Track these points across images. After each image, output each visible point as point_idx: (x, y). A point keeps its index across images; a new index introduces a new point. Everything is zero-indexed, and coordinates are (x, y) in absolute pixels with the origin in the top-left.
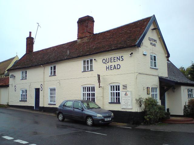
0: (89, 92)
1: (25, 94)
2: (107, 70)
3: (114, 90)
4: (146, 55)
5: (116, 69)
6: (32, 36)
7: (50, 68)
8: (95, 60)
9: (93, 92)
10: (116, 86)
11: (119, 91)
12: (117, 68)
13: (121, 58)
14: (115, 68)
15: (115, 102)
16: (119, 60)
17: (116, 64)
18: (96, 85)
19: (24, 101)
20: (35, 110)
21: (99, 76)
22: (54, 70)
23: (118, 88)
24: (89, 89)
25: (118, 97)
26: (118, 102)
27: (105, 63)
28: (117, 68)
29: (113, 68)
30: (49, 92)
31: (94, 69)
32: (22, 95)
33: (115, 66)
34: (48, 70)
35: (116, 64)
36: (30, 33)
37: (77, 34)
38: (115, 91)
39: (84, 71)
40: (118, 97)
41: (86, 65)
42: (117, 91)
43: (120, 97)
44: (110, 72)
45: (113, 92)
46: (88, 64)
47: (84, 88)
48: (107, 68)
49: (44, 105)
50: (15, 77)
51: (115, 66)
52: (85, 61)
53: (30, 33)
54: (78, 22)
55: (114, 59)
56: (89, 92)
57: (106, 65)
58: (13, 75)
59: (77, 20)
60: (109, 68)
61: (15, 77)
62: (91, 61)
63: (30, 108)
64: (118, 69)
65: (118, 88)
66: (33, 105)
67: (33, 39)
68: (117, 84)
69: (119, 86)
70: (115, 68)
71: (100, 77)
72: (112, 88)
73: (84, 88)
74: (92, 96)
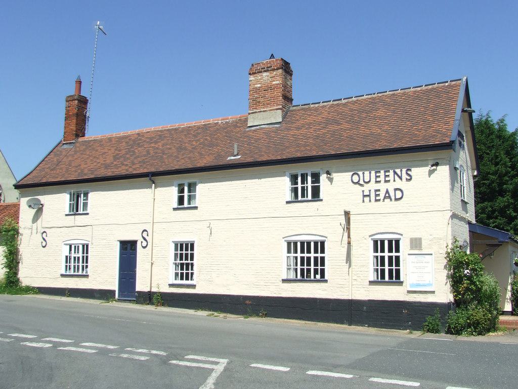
0: (306, 255)
1: (80, 255)
2: (363, 201)
3: (296, 252)
4: (429, 177)
5: (391, 199)
7: (6, 202)
9: (319, 255)
12: (393, 198)
13: (407, 174)
14: (387, 196)
16: (401, 178)
17: (391, 187)
18: (140, 239)
20: (119, 300)
21: (347, 214)
22: (313, 182)
23: (395, 245)
24: (305, 246)
26: (395, 278)
27: (358, 183)
28: (393, 198)
29: (382, 197)
32: (68, 259)
33: (387, 192)
35: (391, 187)
36: (79, 83)
38: (312, 255)
39: (295, 200)
41: (300, 186)
42: (308, 255)
43: (401, 268)
44: (372, 206)
45: (379, 254)
47: (292, 246)
48: (364, 196)
51: (387, 192)
53: (79, 83)
55: (386, 176)
56: (306, 255)
57: (362, 188)
58: (39, 200)
60: (369, 196)
63: (106, 295)
64: (396, 199)
65: (395, 245)
66: (113, 283)
69: (397, 242)
70: (389, 197)
71: (352, 218)
72: (378, 245)
73: (292, 246)
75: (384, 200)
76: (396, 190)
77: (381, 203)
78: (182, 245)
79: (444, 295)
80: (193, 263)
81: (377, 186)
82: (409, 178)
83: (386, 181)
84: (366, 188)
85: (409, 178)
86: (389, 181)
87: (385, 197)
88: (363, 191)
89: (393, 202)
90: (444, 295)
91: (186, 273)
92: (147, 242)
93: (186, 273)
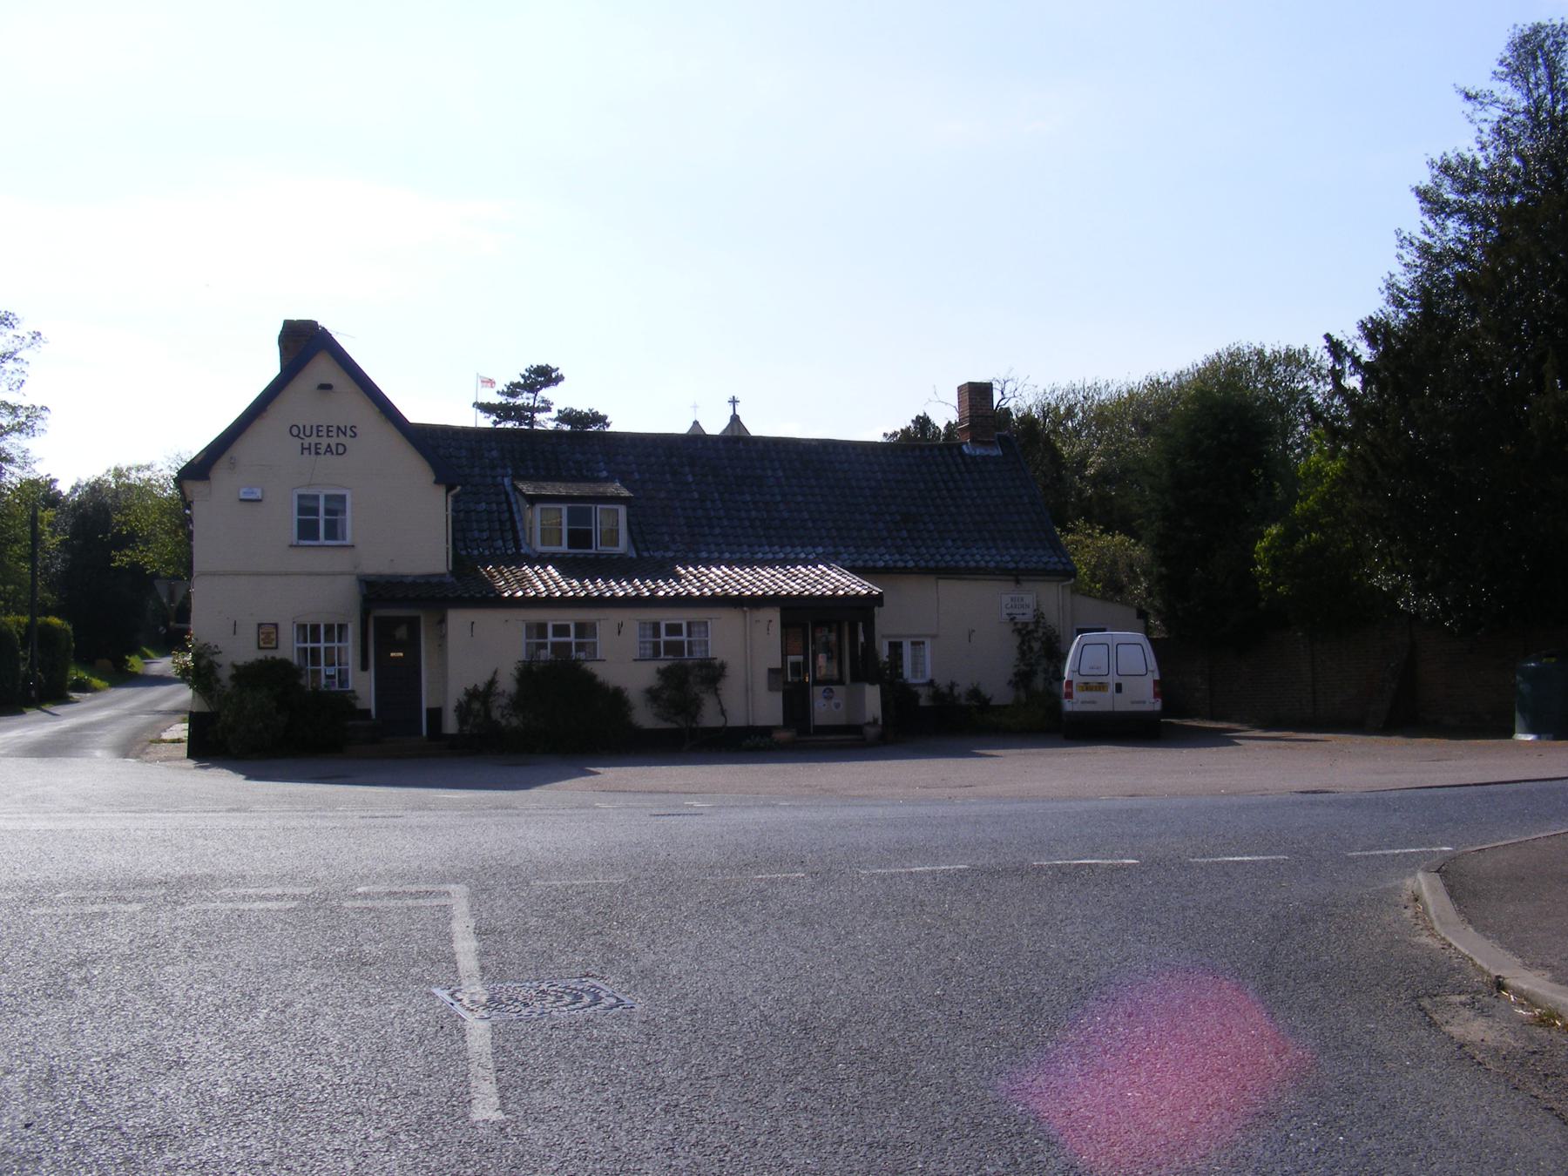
5: (333, 454)
14: (329, 449)
28: (335, 452)
33: (329, 446)
48: (303, 449)
51: (329, 446)
60: (310, 449)
64: (337, 454)
70: (331, 451)
75: (325, 454)
76: (338, 444)
77: (322, 456)
78: (315, 628)
79: (1153, 705)
80: (555, 627)
81: (318, 440)
82: (353, 435)
83: (328, 436)
84: (307, 442)
85: (353, 435)
86: (322, 436)
87: (326, 451)
88: (302, 444)
89: (335, 457)
90: (1153, 705)
91: (319, 642)
92: (726, 719)
93: (319, 642)
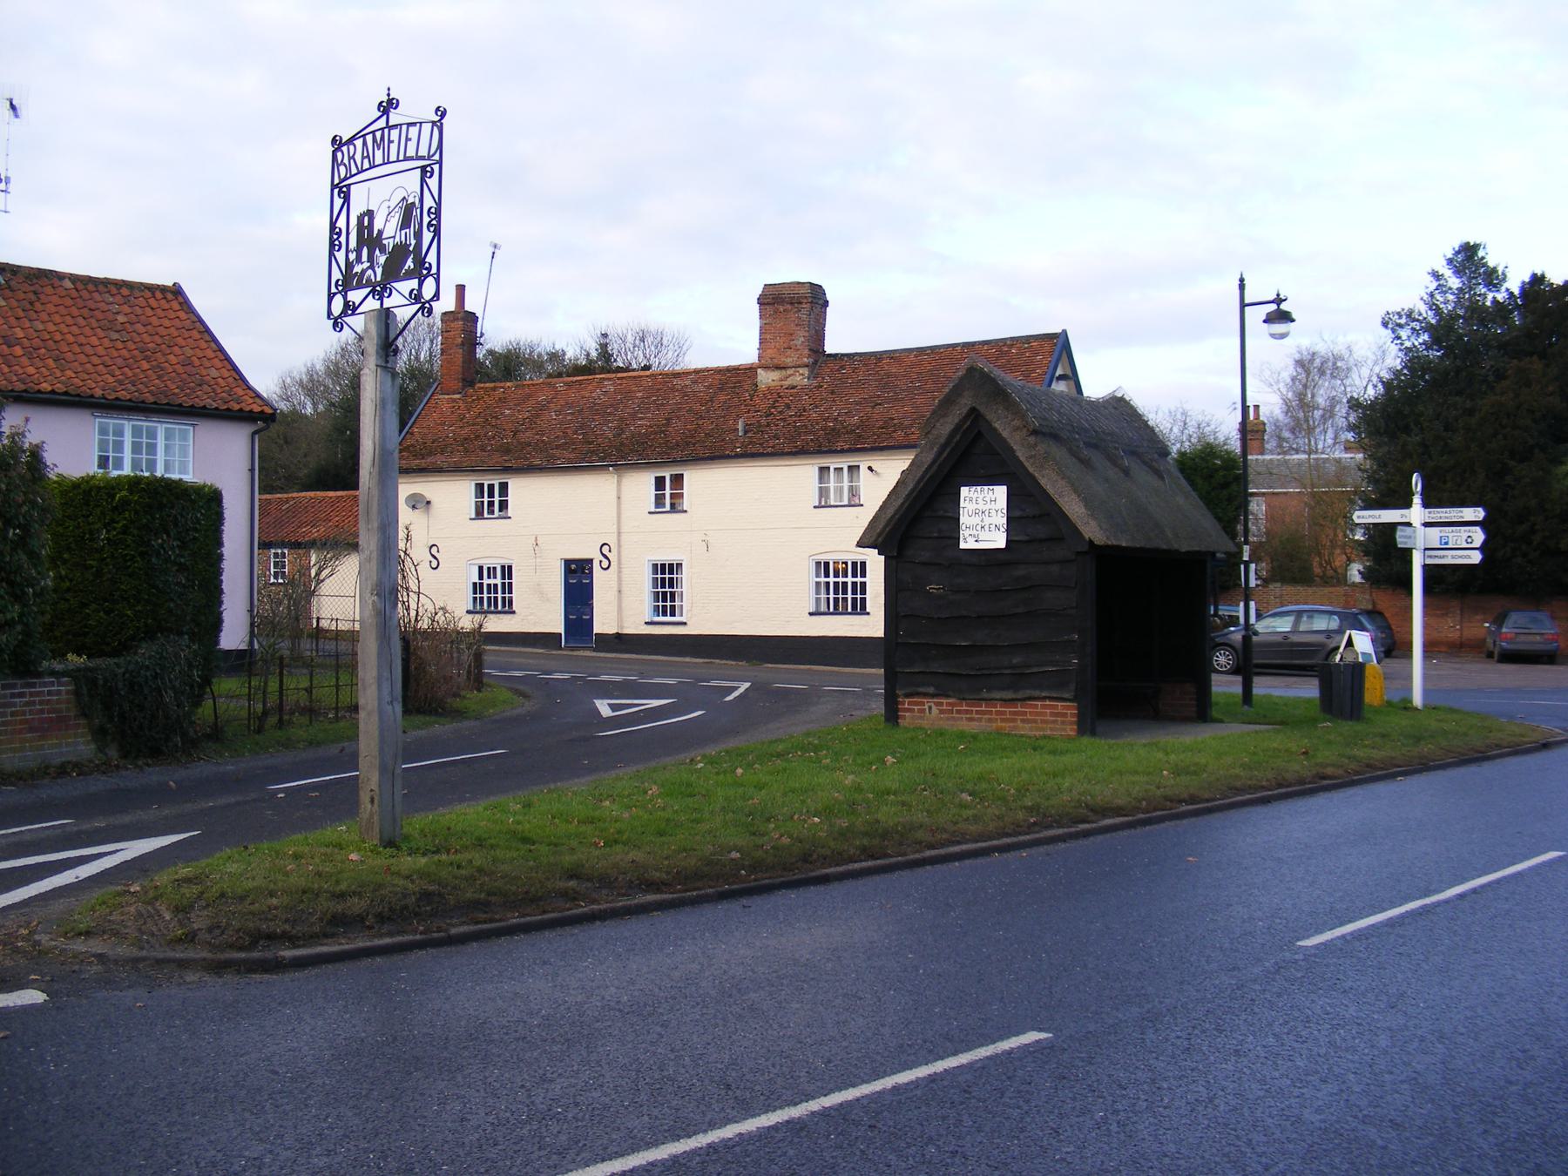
6: (468, 307)
8: (870, 468)
9: (859, 580)
10: (503, 567)
11: (863, 580)
15: (832, 610)
19: (505, 613)
25: (840, 596)
30: (647, 577)
31: (686, 504)
34: (640, 485)
37: (758, 346)
40: (840, 596)
46: (491, 495)
49: (622, 628)
50: (428, 503)
52: (480, 487)
54: (762, 301)
59: (759, 291)
61: (428, 503)
62: (853, 469)
67: (472, 318)
68: (506, 562)
74: (496, 598)
